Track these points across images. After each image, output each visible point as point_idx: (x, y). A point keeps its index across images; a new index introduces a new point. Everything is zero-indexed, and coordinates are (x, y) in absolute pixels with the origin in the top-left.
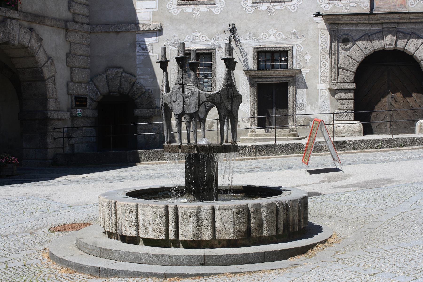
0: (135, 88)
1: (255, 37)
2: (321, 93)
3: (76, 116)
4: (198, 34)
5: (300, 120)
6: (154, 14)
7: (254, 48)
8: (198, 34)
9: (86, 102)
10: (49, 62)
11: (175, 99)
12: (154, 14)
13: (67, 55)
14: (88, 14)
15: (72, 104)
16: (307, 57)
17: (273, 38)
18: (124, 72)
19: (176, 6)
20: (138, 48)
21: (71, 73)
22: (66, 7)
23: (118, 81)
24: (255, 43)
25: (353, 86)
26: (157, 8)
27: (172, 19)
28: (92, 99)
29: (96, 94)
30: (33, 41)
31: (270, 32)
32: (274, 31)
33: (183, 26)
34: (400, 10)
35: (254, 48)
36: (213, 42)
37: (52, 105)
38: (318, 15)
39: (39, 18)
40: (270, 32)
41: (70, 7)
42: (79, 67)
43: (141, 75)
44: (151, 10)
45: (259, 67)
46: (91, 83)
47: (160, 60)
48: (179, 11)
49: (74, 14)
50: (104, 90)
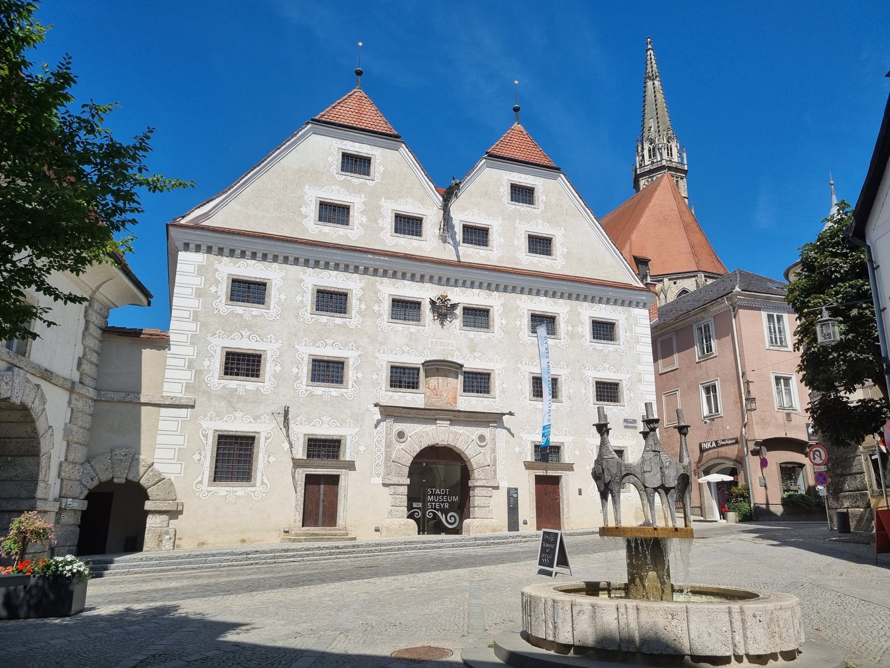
3: (65, 509)
7: (305, 435)
10: (50, 432)
11: (648, 469)
14: (95, 376)
19: (216, 380)
25: (408, 481)
30: (37, 402)
31: (324, 418)
32: (329, 419)
34: (451, 408)
35: (305, 435)
38: (376, 405)
39: (47, 375)
40: (324, 418)
41: (79, 364)
42: (76, 443)
44: (184, 382)
45: (308, 456)
46: (87, 464)
47: (597, 422)
48: (221, 386)
49: (81, 374)
50: (105, 477)
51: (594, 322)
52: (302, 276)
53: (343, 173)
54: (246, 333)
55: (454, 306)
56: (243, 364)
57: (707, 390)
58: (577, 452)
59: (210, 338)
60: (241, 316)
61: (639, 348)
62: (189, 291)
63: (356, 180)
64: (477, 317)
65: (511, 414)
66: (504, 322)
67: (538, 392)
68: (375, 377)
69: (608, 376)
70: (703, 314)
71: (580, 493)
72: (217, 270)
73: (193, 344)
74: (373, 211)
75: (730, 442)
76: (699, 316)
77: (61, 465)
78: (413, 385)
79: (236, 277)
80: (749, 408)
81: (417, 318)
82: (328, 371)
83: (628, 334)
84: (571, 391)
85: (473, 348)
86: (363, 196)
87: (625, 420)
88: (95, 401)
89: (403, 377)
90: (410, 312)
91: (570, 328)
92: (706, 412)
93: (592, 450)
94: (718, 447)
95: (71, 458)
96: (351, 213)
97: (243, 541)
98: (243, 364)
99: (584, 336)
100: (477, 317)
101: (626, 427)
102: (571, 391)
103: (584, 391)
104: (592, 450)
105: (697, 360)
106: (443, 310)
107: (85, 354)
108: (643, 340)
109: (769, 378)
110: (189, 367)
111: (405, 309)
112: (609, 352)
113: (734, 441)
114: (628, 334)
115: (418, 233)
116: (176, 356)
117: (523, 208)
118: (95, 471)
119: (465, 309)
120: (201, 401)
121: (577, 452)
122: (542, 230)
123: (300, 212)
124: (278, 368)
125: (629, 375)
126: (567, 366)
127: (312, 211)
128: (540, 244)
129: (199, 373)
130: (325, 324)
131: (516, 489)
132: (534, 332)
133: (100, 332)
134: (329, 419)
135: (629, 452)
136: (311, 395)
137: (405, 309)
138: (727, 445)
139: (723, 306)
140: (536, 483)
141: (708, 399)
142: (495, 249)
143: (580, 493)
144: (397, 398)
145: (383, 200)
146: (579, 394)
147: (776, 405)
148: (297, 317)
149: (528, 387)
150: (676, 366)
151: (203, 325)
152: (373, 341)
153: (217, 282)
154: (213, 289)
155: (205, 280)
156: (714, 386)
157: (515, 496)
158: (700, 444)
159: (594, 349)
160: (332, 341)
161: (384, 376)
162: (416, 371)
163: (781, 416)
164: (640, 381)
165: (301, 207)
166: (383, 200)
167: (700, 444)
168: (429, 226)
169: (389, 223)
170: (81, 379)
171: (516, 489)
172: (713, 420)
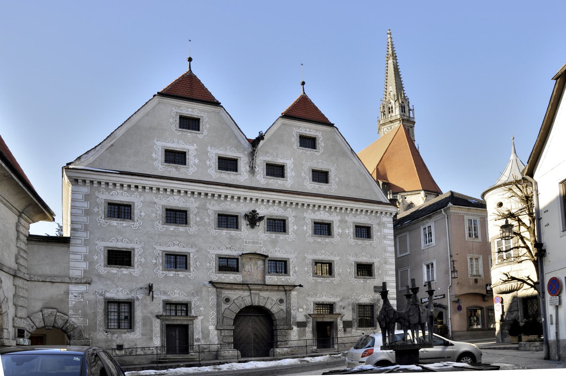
0: (68, 324)
1: (165, 293)
2: (211, 332)
4: (121, 289)
5: (196, 348)
6: (85, 271)
8: (121, 289)
9: (24, 333)
12: (85, 271)
13: (14, 296)
15: (15, 335)
16: (202, 309)
17: (177, 295)
18: (58, 312)
20: (70, 295)
21: (16, 310)
22: (13, 259)
23: (53, 318)
24: (165, 298)
26: (468, 258)
27: (100, 276)
28: (28, 332)
29: (32, 327)
31: (175, 291)
32: (178, 291)
33: (109, 282)
36: (133, 295)
37: (5, 335)
40: (175, 291)
41: (17, 259)
43: (73, 315)
46: (28, 319)
51: (356, 226)
52: (156, 200)
53: (181, 129)
54: (120, 238)
55: (261, 218)
56: (120, 258)
57: (428, 266)
59: (97, 242)
60: (116, 227)
62: (80, 212)
63: (190, 134)
64: (278, 225)
65: (300, 286)
66: (295, 227)
68: (208, 264)
72: (98, 197)
73: (85, 245)
74: (202, 154)
77: (13, 319)
78: (236, 270)
79: (110, 202)
80: (453, 276)
81: (236, 226)
82: (177, 261)
84: (341, 270)
85: (274, 243)
86: (195, 145)
89: (227, 264)
90: (224, 263)
95: (19, 315)
96: (187, 157)
98: (120, 258)
99: (349, 236)
100: (278, 225)
102: (341, 270)
106: (253, 219)
107: (19, 253)
110: (84, 260)
111: (227, 221)
114: (379, 234)
115: (236, 170)
116: (75, 253)
117: (309, 151)
118: (33, 322)
119: (268, 219)
120: (95, 279)
122: (321, 166)
123: (152, 157)
124: (143, 260)
127: (160, 156)
128: (321, 176)
129: (91, 263)
130: (173, 231)
133: (26, 238)
134: (178, 291)
136: (166, 276)
137: (227, 221)
141: (428, 272)
142: (289, 179)
144: (224, 277)
145: (209, 147)
147: (470, 273)
148: (153, 227)
151: (91, 233)
152: (206, 243)
153: (98, 205)
154: (96, 210)
155: (90, 204)
156: (432, 264)
160: (178, 242)
161: (214, 264)
162: (235, 218)
164: (386, 263)
165: (152, 153)
166: (209, 147)
168: (242, 165)
169: (214, 163)
170: (18, 268)
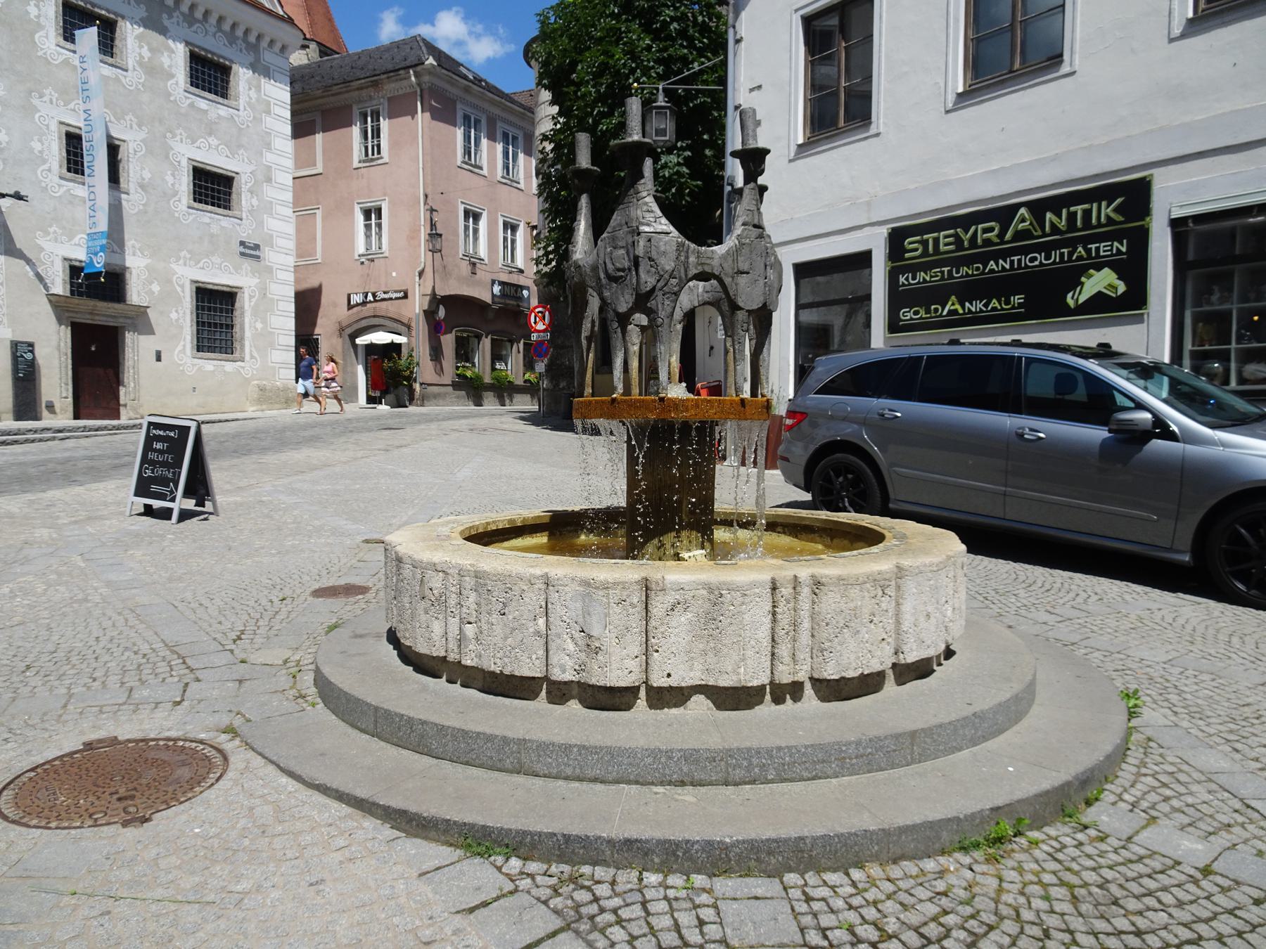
45: (72, 292)
57: (367, 214)
58: (156, 288)
61: (269, 121)
65: (18, 196)
67: (75, 161)
69: (218, 161)
70: (371, 91)
71: (159, 359)
75: (394, 295)
76: (364, 93)
83: (253, 93)
87: (242, 243)
88: (1177, 519)
91: (146, 53)
92: (361, 248)
93: (182, 286)
94: (376, 301)
97: (421, 274)
99: (172, 76)
101: (242, 254)
103: (170, 179)
104: (182, 286)
105: (356, 164)
108: (278, 110)
109: (457, 208)
112: (219, 117)
113: (402, 294)
121: (156, 288)
125: (252, 168)
126: (140, 126)
131: (31, 345)
132: (69, 36)
135: (246, 296)
138: (391, 299)
139: (405, 83)
140: (870, 92)
141: (368, 227)
143: (159, 359)
146: (159, 180)
147: (461, 252)
149: (56, 151)
150: (320, 170)
156: (379, 211)
157: (29, 356)
158: (349, 296)
159: (192, 105)
163: (465, 267)
167: (349, 296)
171: (31, 345)
172: (372, 260)
